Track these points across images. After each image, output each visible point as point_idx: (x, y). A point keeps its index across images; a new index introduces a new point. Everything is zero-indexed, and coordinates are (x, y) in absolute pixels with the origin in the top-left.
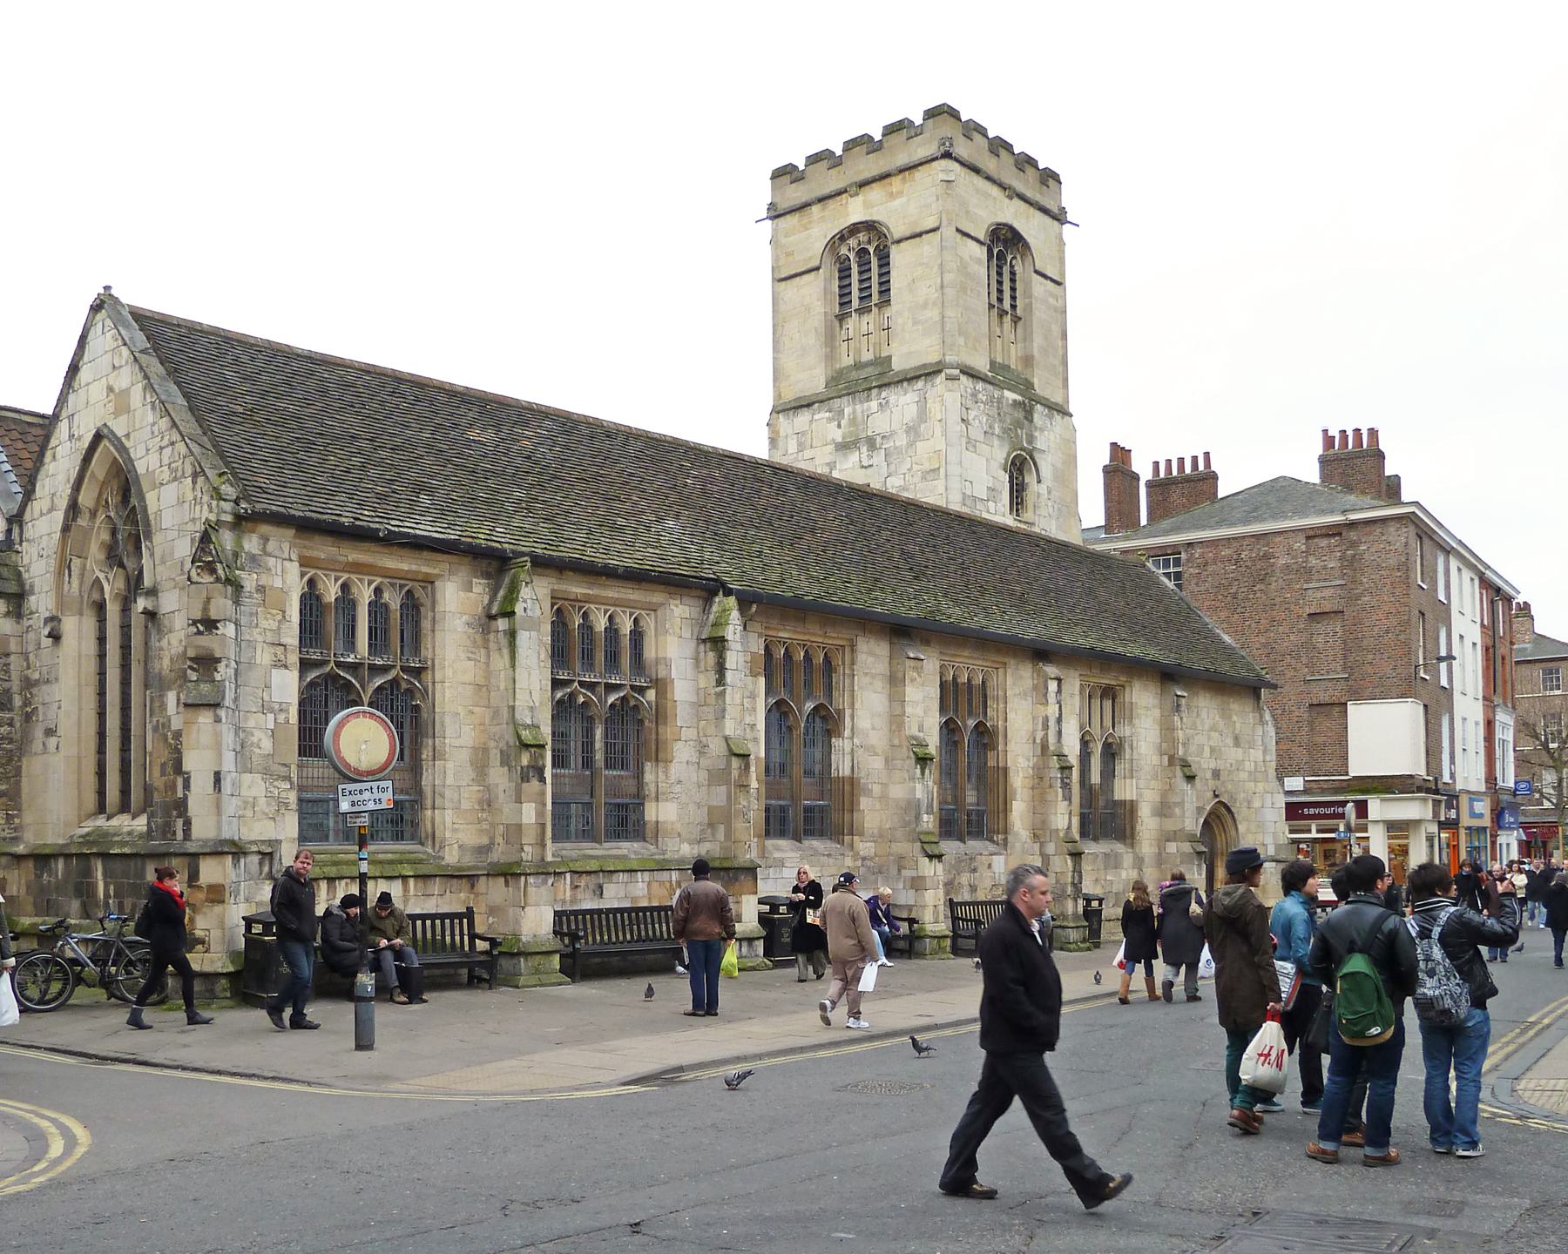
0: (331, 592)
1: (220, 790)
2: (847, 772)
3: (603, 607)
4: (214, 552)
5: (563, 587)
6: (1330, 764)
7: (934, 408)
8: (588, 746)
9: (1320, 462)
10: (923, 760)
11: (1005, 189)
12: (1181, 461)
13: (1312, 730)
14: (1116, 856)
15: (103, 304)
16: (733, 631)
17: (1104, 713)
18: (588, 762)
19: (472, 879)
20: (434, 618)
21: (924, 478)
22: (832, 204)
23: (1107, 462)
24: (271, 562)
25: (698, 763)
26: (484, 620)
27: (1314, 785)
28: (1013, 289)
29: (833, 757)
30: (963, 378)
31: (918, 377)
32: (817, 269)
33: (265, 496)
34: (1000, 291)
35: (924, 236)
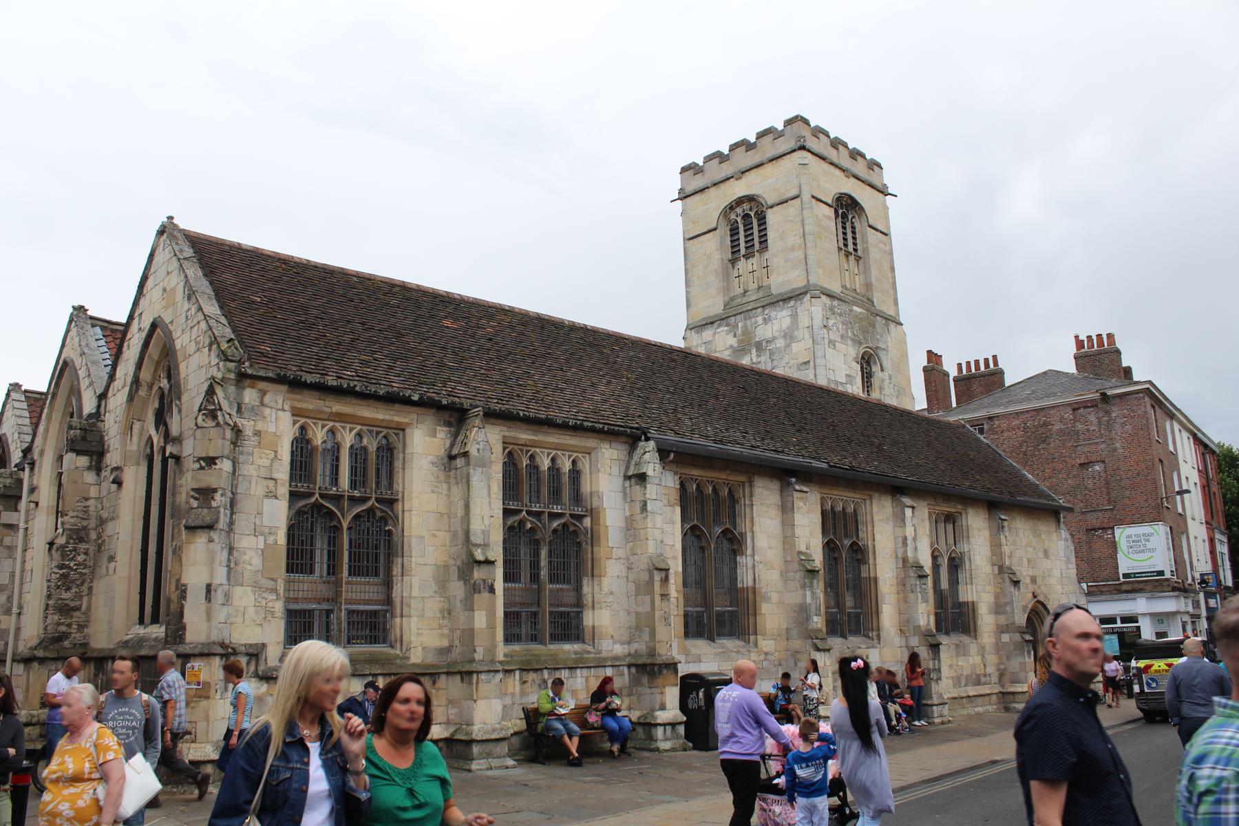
0: (319, 436)
1: (210, 600)
2: (750, 583)
3: (546, 451)
4: (216, 401)
5: (513, 434)
6: (1106, 573)
7: (804, 321)
8: (535, 565)
9: (1075, 358)
10: (812, 572)
11: (844, 171)
12: (977, 362)
13: (1090, 547)
14: (964, 646)
15: (167, 230)
16: (652, 467)
17: (939, 533)
18: (535, 578)
19: (434, 676)
20: (404, 459)
21: (799, 369)
22: (723, 186)
23: (926, 364)
24: (267, 411)
25: (627, 578)
26: (446, 460)
27: (1094, 589)
28: (854, 238)
29: (738, 571)
30: (824, 298)
31: (790, 298)
32: (715, 229)
33: (264, 359)
34: (845, 239)
35: (789, 202)
